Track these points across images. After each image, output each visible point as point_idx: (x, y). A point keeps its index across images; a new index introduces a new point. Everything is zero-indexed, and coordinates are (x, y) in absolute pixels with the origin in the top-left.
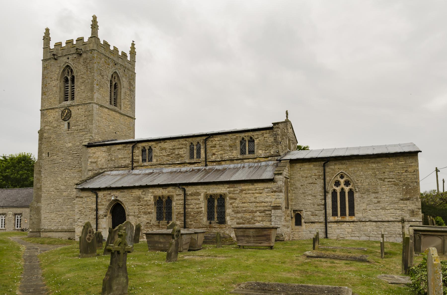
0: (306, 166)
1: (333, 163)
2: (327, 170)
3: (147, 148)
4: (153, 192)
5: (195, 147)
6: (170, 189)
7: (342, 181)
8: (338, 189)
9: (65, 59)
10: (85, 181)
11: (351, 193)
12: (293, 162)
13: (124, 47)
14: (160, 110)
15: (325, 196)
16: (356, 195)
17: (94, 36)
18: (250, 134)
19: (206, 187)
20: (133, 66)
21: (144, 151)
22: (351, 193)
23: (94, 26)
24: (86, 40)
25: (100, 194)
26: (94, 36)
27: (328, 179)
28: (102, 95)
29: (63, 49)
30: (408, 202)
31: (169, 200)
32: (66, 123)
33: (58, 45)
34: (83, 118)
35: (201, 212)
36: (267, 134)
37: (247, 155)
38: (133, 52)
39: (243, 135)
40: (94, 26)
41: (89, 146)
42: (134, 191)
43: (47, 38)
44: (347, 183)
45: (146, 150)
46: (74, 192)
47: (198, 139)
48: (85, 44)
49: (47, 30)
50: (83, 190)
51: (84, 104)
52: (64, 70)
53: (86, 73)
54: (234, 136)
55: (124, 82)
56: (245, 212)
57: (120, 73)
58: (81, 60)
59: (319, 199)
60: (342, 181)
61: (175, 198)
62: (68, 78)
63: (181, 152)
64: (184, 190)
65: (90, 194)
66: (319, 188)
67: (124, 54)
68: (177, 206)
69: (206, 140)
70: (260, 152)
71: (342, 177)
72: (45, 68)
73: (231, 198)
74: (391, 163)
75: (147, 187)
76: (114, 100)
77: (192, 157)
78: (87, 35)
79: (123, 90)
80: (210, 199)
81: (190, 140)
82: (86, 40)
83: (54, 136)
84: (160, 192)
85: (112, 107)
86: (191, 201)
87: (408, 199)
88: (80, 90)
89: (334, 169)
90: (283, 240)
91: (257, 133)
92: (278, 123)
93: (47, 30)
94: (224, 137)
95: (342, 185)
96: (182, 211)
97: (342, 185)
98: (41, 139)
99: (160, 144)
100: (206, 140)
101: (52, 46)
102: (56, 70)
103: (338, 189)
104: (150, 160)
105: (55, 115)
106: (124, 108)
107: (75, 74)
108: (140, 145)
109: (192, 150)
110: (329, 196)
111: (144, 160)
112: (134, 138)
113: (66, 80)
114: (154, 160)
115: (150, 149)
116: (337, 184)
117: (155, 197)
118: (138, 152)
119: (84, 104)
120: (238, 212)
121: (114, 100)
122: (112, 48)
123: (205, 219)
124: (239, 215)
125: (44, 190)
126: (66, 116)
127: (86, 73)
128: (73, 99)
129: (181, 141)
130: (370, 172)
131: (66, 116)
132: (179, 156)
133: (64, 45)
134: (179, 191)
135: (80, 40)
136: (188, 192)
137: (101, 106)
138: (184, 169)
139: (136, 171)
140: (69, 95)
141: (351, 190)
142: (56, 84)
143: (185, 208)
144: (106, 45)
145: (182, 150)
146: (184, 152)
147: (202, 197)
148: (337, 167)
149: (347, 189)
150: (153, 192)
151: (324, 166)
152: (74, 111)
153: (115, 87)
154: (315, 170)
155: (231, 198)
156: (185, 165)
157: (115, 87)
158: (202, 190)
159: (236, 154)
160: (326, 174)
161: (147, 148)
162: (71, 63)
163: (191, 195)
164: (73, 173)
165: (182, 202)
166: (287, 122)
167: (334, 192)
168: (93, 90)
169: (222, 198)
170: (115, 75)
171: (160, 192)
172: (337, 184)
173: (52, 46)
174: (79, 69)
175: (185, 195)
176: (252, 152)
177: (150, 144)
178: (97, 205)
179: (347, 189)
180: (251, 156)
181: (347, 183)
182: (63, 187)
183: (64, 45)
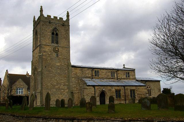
6: (120, 87)
16: (151, 91)
17: (42, 14)
19: (130, 87)
21: (96, 72)
23: (41, 11)
25: (96, 87)
26: (42, 14)
31: (119, 91)
37: (128, 78)
40: (41, 11)
42: (108, 87)
47: (114, 70)
49: (41, 7)
53: (51, 32)
56: (140, 95)
64: (125, 88)
65: (91, 87)
68: (122, 93)
73: (136, 91)
77: (112, 76)
80: (131, 91)
84: (117, 88)
93: (41, 7)
96: (124, 94)
99: (102, 70)
106: (62, 43)
109: (112, 74)
115: (98, 72)
117: (115, 90)
118: (93, 72)
120: (138, 95)
124: (139, 96)
127: (51, 32)
129: (109, 70)
134: (123, 88)
136: (126, 88)
147: (129, 90)
155: (136, 91)
158: (129, 88)
159: (125, 77)
163: (126, 89)
164: (61, 77)
165: (124, 92)
169: (134, 90)
171: (117, 88)
176: (129, 77)
178: (95, 92)
180: (129, 78)
183: (58, 18)
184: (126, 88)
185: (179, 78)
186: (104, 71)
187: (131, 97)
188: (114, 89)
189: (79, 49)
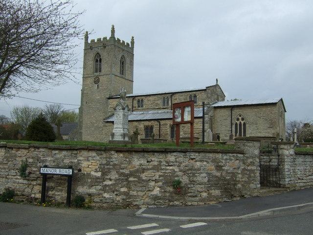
0: (223, 110)
1: (236, 108)
2: (233, 112)
3: (140, 100)
4: (143, 124)
5: (166, 100)
6: (152, 122)
7: (240, 118)
8: (238, 122)
9: (96, 49)
10: (108, 118)
11: (244, 124)
12: (215, 108)
13: (128, 41)
14: (147, 78)
15: (232, 126)
16: (247, 125)
18: (194, 93)
20: (132, 48)
21: (139, 101)
22: (244, 124)
23: (113, 31)
24: (108, 39)
27: (233, 117)
28: (117, 70)
29: (96, 43)
30: (271, 129)
31: (152, 127)
32: (96, 85)
33: (93, 41)
34: (106, 83)
35: (167, 134)
36: (203, 93)
38: (133, 43)
39: (191, 93)
40: (113, 31)
41: (109, 98)
42: (134, 123)
43: (87, 37)
44: (243, 119)
45: (140, 101)
46: (101, 125)
47: (168, 95)
48: (107, 41)
49: (113, 26)
50: (108, 122)
51: (107, 75)
52: (95, 56)
54: (186, 94)
55: (128, 60)
57: (126, 56)
58: (106, 50)
59: (229, 128)
60: (240, 118)
61: (155, 126)
62: (98, 60)
63: (159, 102)
66: (229, 122)
67: (128, 44)
68: (155, 131)
69: (171, 96)
70: (200, 102)
71: (240, 116)
72: (85, 54)
74: (264, 109)
75: (140, 120)
76: (122, 72)
77: (164, 105)
78: (109, 36)
79: (127, 65)
81: (163, 95)
82: (108, 39)
83: (90, 92)
84: (147, 123)
85: (121, 76)
86: (163, 128)
87: (271, 128)
88: (105, 68)
89: (236, 112)
90: (279, 186)
91: (198, 92)
92: (209, 87)
93: (113, 26)
94: (181, 94)
95: (240, 120)
97: (240, 120)
98: (82, 94)
100: (171, 96)
101: (89, 42)
102: (92, 56)
103: (238, 122)
104: (142, 106)
105: (90, 81)
106: (127, 72)
107: (101, 57)
108: (137, 98)
110: (234, 126)
111: (139, 106)
112: (132, 93)
113: (97, 61)
114: (144, 107)
115: (142, 100)
116: (238, 119)
117: (144, 126)
118: (135, 102)
119: (107, 75)
121: (122, 72)
122: (121, 42)
123: (170, 137)
125: (84, 123)
126: (97, 81)
128: (100, 71)
129: (159, 96)
130: (254, 113)
131: (97, 81)
132: (157, 104)
133: (96, 41)
134: (156, 123)
135: (105, 38)
136: (161, 124)
137: (116, 76)
138: (160, 112)
139: (134, 113)
140: (98, 69)
141: (244, 123)
142: (91, 63)
143: (159, 132)
144: (119, 40)
145: (159, 101)
146: (160, 102)
147: (168, 126)
148: (238, 110)
149: (242, 122)
150: (143, 124)
151: (231, 110)
152: (101, 78)
153: (122, 64)
154: (227, 112)
156: (98, 148)
157: (122, 64)
160: (233, 114)
161: (140, 100)
162: (100, 51)
166: (217, 86)
167: (236, 124)
168: (109, 66)
170: (123, 57)
171: (147, 123)
172: (238, 119)
173: (89, 42)
174: (104, 55)
175: (160, 124)
177: (142, 97)
179: (242, 122)
181: (243, 119)
182: (94, 121)
183: (96, 41)
184: (162, 122)
185: (151, 169)
186: (151, 98)
187: (172, 137)
188: (142, 126)
189: (147, 78)
